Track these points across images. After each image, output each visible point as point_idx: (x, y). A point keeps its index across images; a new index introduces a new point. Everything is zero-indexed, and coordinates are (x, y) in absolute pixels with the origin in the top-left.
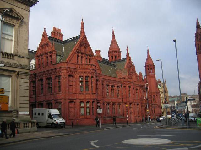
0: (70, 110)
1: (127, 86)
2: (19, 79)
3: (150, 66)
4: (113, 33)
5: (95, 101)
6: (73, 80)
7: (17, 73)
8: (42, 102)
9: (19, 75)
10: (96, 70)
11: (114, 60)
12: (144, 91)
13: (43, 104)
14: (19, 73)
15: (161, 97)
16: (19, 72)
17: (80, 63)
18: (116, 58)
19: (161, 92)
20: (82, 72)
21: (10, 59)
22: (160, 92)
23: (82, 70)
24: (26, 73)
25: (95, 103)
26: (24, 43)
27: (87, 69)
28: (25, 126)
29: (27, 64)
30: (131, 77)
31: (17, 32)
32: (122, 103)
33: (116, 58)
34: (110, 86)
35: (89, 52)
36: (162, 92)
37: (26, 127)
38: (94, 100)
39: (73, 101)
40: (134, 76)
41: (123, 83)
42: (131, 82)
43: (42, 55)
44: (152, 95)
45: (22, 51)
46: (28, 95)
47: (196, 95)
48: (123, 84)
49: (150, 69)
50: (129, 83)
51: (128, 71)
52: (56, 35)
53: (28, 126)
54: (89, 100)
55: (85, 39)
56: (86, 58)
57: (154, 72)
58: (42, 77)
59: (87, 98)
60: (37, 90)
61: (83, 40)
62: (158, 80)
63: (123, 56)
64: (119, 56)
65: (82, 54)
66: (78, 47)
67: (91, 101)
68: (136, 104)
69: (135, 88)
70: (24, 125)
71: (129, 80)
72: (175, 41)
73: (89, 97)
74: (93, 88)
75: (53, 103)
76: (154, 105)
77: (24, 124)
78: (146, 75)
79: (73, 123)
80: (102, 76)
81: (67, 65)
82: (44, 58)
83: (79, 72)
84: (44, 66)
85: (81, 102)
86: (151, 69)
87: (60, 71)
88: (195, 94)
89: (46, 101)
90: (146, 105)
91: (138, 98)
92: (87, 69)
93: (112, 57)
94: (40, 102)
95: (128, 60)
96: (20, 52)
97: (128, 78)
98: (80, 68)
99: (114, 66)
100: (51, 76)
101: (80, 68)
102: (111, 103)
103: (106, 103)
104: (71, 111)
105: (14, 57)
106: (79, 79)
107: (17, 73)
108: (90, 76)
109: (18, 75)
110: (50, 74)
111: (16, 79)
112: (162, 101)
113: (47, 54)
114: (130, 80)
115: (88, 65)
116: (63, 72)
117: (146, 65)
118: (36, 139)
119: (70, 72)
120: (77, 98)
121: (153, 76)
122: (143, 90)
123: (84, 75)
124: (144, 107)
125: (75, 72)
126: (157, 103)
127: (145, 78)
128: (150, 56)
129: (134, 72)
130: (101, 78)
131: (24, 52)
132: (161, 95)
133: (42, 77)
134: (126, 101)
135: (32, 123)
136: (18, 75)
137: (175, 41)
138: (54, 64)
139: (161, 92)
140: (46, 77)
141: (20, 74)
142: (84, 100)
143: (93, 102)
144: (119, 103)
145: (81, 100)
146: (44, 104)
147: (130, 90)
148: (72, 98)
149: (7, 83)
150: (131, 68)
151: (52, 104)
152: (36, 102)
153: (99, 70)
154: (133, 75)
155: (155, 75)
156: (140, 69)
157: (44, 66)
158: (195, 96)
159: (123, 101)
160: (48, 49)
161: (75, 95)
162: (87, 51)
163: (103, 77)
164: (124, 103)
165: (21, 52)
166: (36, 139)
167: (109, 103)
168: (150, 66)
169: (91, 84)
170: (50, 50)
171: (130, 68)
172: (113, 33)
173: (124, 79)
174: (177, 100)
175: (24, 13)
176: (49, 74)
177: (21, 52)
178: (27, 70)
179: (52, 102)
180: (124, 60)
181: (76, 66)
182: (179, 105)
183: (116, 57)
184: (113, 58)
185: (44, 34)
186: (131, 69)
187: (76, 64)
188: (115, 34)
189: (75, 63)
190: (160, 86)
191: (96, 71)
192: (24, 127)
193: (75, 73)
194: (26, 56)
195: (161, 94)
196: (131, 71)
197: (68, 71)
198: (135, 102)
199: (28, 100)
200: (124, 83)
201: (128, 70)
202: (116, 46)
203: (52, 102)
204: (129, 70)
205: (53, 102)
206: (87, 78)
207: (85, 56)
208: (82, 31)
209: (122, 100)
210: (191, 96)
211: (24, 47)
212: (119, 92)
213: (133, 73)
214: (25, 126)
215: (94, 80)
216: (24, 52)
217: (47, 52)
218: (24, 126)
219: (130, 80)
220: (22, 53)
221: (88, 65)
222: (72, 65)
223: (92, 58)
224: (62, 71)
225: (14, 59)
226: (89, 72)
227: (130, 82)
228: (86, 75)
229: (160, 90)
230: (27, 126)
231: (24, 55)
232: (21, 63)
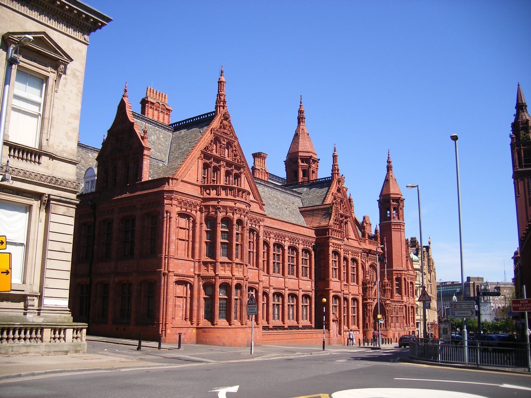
0: (177, 303)
4: (300, 112)
10: (251, 203)
16: (51, 197)
21: (35, 162)
24: (68, 200)
26: (69, 123)
28: (57, 336)
30: (341, 227)
34: (286, 248)
39: (185, 279)
45: (61, 143)
46: (69, 257)
47: (508, 284)
53: (41, 339)
55: (225, 122)
56: (228, 174)
60: (95, 247)
62: (412, 238)
63: (323, 172)
65: (217, 160)
70: (54, 334)
72: (455, 138)
77: (54, 330)
79: (182, 337)
80: (266, 219)
88: (40, 145)
90: (375, 303)
102: (286, 293)
103: (273, 291)
105: (39, 159)
118: (89, 370)
122: (370, 263)
124: (174, 332)
127: (376, 231)
129: (348, 214)
135: (74, 329)
137: (455, 138)
144: (307, 293)
148: (184, 273)
149: (9, 223)
152: (217, 277)
154: (346, 223)
158: (504, 284)
162: (227, 154)
163: (268, 222)
165: (58, 146)
174: (458, 295)
175: (73, 47)
177: (58, 146)
182: (458, 307)
188: (305, 115)
192: (54, 338)
194: (72, 157)
208: (220, 102)
210: (494, 286)
211: (67, 133)
213: (346, 218)
214: (57, 336)
216: (66, 147)
218: (53, 336)
220: (61, 148)
222: (189, 186)
225: (39, 163)
230: (62, 335)
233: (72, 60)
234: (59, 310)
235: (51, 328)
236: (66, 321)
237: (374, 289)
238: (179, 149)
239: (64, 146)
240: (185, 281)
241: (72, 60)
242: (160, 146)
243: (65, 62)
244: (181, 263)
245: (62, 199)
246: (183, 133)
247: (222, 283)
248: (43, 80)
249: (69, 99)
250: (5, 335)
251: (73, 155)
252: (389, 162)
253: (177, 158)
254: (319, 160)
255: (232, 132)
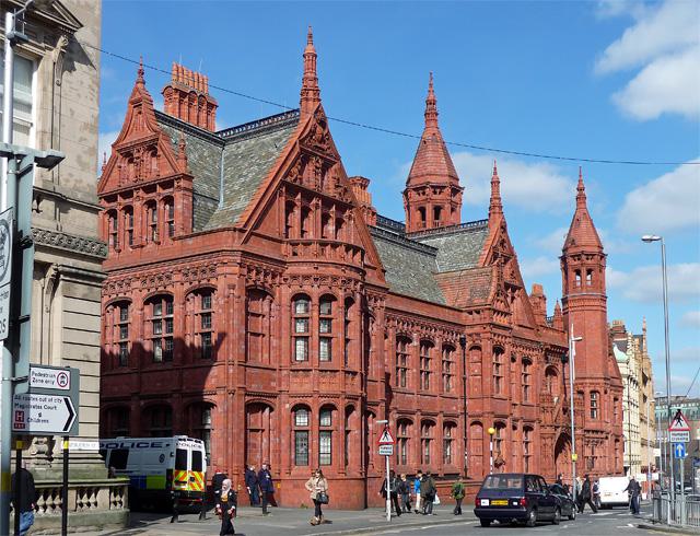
1: (487, 347)
2: (59, 298)
3: (582, 261)
5: (358, 404)
6: (266, 309)
7: (53, 272)
8: (127, 399)
9: (61, 283)
11: (429, 226)
12: (551, 372)
13: (128, 409)
14: (59, 273)
15: (625, 398)
17: (294, 235)
18: (437, 216)
19: (625, 380)
20: (306, 277)
22: (619, 377)
23: (305, 269)
25: (356, 414)
26: (81, 139)
27: (326, 264)
29: (92, 235)
31: (50, 88)
32: (460, 421)
33: (437, 216)
35: (337, 187)
36: (628, 377)
37: (89, 504)
38: (352, 402)
40: (518, 301)
41: (468, 331)
42: (504, 328)
43: (127, 194)
44: (587, 390)
45: (71, 175)
48: (470, 335)
49: (584, 272)
50: (495, 330)
51: (495, 279)
52: (186, 100)
54: (332, 401)
57: (599, 284)
58: (125, 288)
59: (324, 389)
61: (313, 132)
64: (453, 210)
66: (293, 165)
67: (341, 404)
68: (520, 425)
69: (519, 358)
71: (498, 319)
73: (307, 388)
74: (348, 349)
75: (175, 407)
76: (591, 435)
78: (565, 301)
81: (246, 242)
82: (137, 205)
83: (295, 277)
84: (134, 244)
85: (296, 408)
86: (589, 272)
87: (212, 270)
89: (141, 398)
91: (501, 395)
92: (326, 264)
93: (423, 210)
94: (115, 399)
95: (496, 226)
96: (62, 182)
97: (495, 311)
98: (295, 259)
99: (432, 252)
100: (169, 289)
101: (295, 259)
104: (255, 446)
106: (291, 310)
107: (53, 272)
108: (341, 294)
109: (55, 282)
110: (165, 281)
111: (47, 298)
112: (626, 414)
113: (150, 189)
114: (503, 321)
115: (335, 246)
116: (225, 275)
117: (413, 182)
119: (253, 274)
120: (283, 388)
121: (596, 303)
123: (315, 291)
125: (274, 277)
126: (609, 428)
128: (586, 216)
129: (517, 284)
130: (384, 304)
131: (81, 181)
132: (625, 392)
133: (125, 288)
134: (478, 411)
135: (110, 488)
136: (55, 282)
138: (181, 234)
139: (625, 380)
140: (145, 292)
141: (62, 276)
142: (309, 401)
143: (349, 410)
144: (451, 419)
145: (298, 401)
146: (133, 408)
147: (498, 365)
150: (508, 266)
151: (168, 409)
153: (375, 269)
154: (513, 298)
155: (604, 298)
156: (541, 271)
157: (134, 244)
159: (465, 408)
160: (154, 167)
161: (275, 375)
164: (470, 420)
165: (67, 181)
166: (458, 524)
167: (408, 416)
168: (584, 257)
169: (341, 330)
170: (167, 172)
171: (505, 263)
172: (431, 103)
173: (478, 312)
176: (160, 279)
177: (67, 181)
178: (498, 322)
179: (169, 401)
180: (477, 227)
181: (280, 250)
183: (437, 210)
184: (424, 218)
185: (137, 96)
186: (507, 269)
187: (281, 242)
189: (276, 236)
190: (624, 348)
191: (364, 273)
193: (277, 280)
194: (91, 200)
195: (623, 388)
196: (507, 278)
197: (245, 271)
198: (516, 415)
199: (98, 389)
200: (477, 329)
201: (495, 274)
202: (443, 160)
203: (169, 401)
204: (500, 277)
205: (176, 403)
206: (325, 308)
207: (317, 206)
208: (310, 91)
209: (460, 405)
211: (79, 157)
212: (453, 369)
215: (354, 312)
216: (81, 181)
217: (148, 179)
219: (503, 321)
220: (71, 184)
221: (335, 246)
222: (264, 241)
223: (350, 218)
224: (219, 270)
226: (335, 279)
227: (499, 327)
228: (324, 289)
229: (623, 370)
231: (79, 196)
232: (68, 229)
233: (82, 26)
234: (89, 458)
235: (110, 488)
236: (98, 474)
237: (556, 411)
238: (240, 176)
239: (76, 181)
240: (259, 403)
241: (82, 26)
242: (206, 173)
243: (69, 29)
244: (257, 374)
245: (81, 272)
246: (243, 148)
247: (324, 405)
248: (31, 62)
249: (79, 95)
250: (40, 502)
251: (92, 196)
252: (580, 189)
253: (239, 192)
254: (463, 189)
255: (332, 146)
